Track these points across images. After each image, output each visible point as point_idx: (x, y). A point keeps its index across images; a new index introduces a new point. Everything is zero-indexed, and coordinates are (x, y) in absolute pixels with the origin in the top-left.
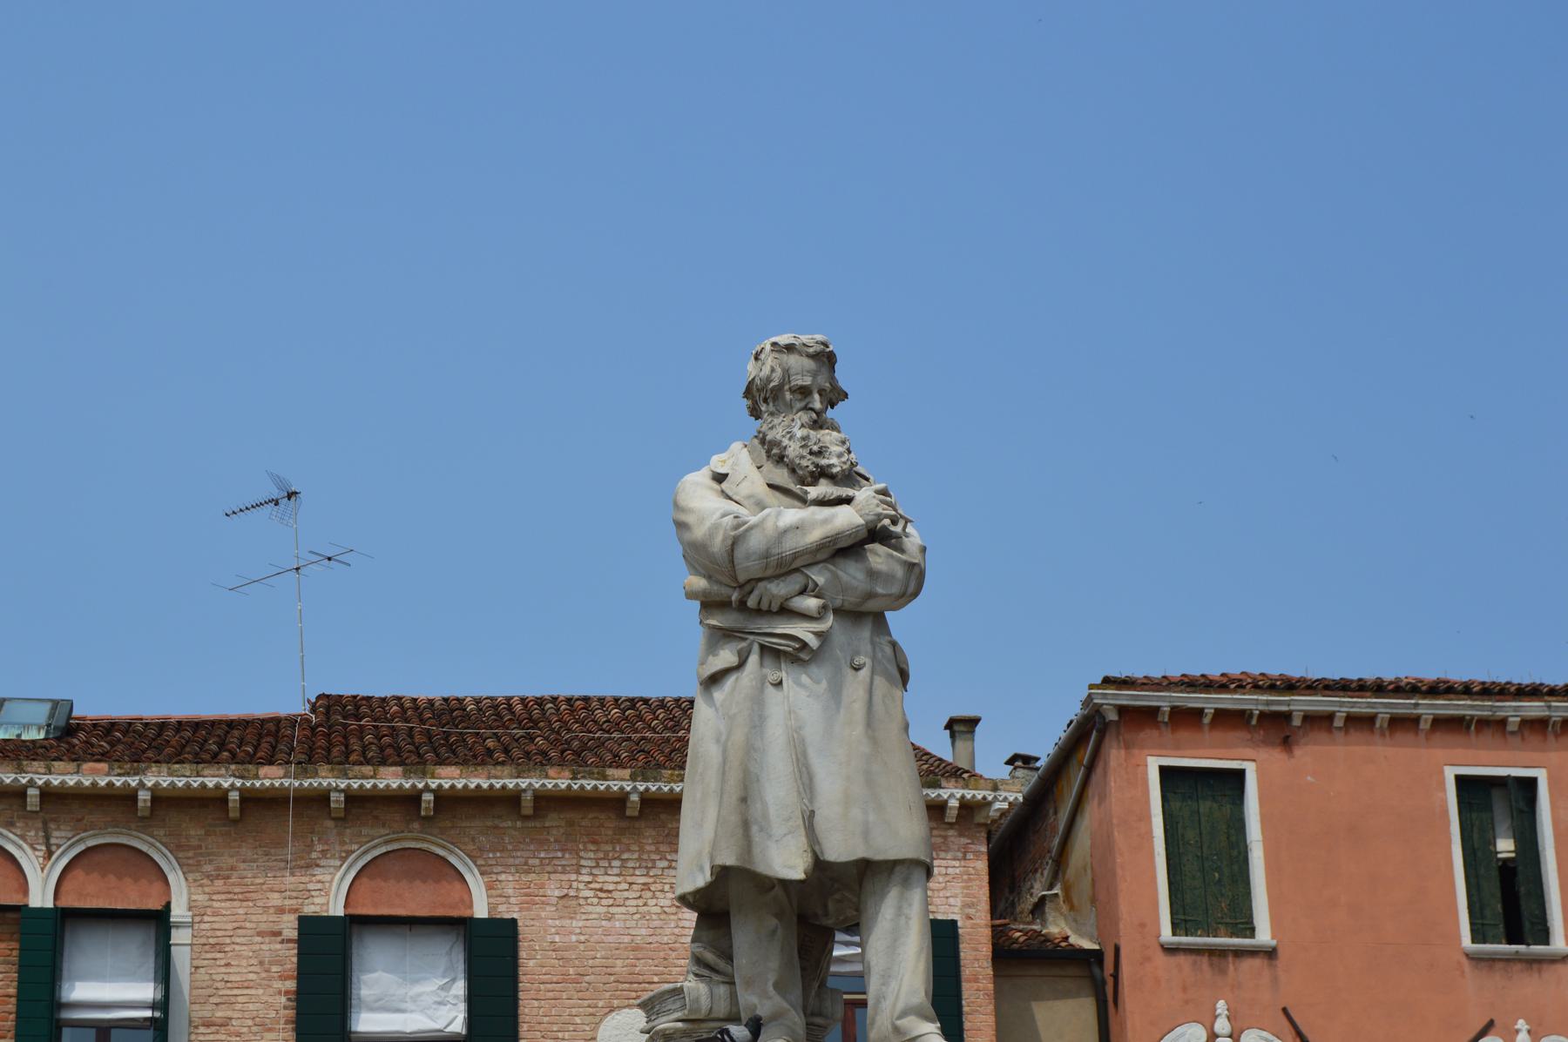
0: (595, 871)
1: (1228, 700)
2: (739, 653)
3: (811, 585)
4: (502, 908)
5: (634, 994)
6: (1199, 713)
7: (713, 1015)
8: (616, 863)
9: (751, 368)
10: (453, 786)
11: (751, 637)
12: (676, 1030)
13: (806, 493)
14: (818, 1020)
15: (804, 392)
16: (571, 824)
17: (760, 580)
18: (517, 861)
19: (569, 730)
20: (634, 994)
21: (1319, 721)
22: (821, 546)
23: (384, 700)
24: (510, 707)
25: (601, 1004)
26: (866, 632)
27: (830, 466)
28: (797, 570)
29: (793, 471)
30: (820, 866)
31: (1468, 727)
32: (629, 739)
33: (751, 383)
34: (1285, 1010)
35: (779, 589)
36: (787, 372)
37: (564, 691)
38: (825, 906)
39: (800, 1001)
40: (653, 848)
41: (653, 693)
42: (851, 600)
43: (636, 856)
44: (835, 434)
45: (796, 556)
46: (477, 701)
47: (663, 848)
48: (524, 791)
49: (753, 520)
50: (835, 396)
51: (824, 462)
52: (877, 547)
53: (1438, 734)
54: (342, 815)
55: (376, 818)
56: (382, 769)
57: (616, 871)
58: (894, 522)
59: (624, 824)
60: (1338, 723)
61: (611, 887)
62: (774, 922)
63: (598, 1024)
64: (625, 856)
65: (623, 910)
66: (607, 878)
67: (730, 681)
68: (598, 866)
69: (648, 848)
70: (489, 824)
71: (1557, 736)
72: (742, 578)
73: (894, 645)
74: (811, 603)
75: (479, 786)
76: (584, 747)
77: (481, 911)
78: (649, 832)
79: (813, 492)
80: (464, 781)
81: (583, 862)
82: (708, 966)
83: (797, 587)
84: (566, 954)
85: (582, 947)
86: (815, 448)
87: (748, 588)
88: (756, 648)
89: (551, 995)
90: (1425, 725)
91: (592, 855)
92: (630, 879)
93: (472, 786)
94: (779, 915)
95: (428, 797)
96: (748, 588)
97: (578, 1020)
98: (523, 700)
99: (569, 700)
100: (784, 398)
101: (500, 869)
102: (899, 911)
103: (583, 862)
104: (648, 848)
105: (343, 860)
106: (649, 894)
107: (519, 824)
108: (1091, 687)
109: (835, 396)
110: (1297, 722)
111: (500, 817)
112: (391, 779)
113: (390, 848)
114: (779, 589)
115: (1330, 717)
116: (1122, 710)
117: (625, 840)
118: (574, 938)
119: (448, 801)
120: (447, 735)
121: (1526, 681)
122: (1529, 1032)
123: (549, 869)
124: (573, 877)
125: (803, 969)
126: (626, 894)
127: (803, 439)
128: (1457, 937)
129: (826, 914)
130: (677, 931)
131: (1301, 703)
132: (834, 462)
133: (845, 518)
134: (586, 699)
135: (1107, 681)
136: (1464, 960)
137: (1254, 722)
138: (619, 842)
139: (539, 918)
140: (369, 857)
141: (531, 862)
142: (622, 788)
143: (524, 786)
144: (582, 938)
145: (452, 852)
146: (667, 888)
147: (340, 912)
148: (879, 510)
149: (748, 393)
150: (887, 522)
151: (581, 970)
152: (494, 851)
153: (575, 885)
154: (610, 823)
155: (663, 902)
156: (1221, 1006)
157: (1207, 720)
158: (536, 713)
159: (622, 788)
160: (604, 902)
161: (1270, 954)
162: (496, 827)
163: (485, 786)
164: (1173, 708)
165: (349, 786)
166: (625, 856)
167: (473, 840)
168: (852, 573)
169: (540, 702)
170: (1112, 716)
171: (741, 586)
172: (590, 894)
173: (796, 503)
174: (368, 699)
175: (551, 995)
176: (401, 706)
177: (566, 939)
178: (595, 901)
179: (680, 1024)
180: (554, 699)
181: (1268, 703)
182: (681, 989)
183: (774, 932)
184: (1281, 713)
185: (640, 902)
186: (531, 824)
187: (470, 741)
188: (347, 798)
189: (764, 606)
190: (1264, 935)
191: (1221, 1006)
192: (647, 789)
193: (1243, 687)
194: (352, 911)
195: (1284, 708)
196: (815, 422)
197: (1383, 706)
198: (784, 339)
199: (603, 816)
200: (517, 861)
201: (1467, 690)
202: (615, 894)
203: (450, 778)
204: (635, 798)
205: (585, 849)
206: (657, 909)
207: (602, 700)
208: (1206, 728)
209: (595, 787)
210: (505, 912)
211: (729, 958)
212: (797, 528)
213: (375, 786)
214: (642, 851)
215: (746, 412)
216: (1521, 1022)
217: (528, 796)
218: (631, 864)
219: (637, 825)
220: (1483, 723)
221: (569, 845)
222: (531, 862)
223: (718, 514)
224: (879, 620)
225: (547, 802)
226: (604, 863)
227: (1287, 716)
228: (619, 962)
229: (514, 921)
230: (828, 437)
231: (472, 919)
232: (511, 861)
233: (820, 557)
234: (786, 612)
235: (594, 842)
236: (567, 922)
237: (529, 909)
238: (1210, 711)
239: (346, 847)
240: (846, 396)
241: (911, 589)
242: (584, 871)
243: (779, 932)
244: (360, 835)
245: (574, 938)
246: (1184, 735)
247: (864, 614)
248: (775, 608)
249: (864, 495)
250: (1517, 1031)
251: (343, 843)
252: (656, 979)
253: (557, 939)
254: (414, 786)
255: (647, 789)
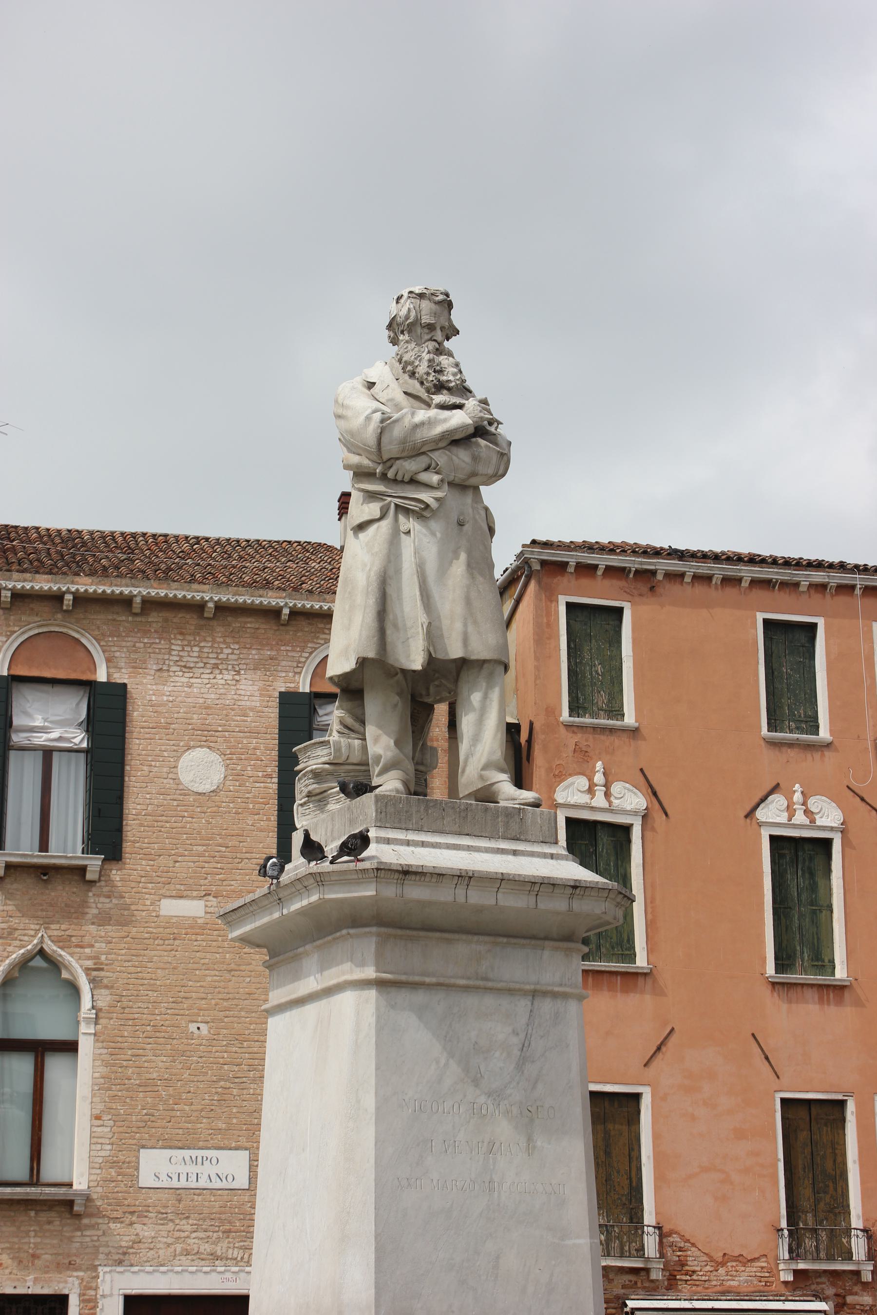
0: (181, 654)
1: (615, 560)
2: (381, 509)
3: (433, 465)
4: (116, 675)
5: (204, 738)
6: (595, 567)
7: (349, 761)
8: (196, 649)
9: (393, 309)
10: (86, 591)
11: (389, 499)
12: (324, 770)
13: (432, 399)
14: (421, 768)
15: (431, 327)
16: (166, 620)
17: (398, 459)
18: (128, 644)
19: (157, 556)
20: (204, 738)
21: (676, 577)
22: (443, 436)
23: (26, 528)
24: (114, 539)
25: (182, 744)
26: (469, 499)
27: (449, 381)
28: (424, 453)
29: (422, 383)
30: (431, 661)
31: (774, 587)
32: (198, 565)
33: (393, 319)
34: (641, 770)
35: (410, 466)
36: (419, 311)
37: (151, 529)
38: (428, 689)
39: (411, 754)
40: (221, 640)
41: (213, 534)
42: (460, 476)
43: (210, 644)
44: (451, 359)
45: (424, 443)
46: (91, 533)
47: (228, 640)
48: (135, 596)
49: (396, 416)
50: (452, 332)
51: (444, 378)
52: (480, 440)
53: (754, 590)
54: (9, 606)
55: (32, 609)
56: (37, 576)
57: (196, 654)
58: (490, 424)
59: (202, 622)
60: (688, 579)
61: (192, 665)
62: (397, 698)
63: (179, 757)
64: (202, 644)
65: (199, 680)
66: (189, 659)
67: (372, 530)
68: (183, 650)
69: (218, 639)
70: (110, 617)
71: (832, 596)
72: (385, 457)
73: (487, 509)
74: (435, 478)
75: (104, 591)
76: (169, 569)
77: (102, 676)
78: (219, 629)
79: (438, 399)
80: (94, 588)
81: (173, 647)
82: (346, 727)
83: (424, 466)
84: (159, 709)
85: (170, 705)
86: (438, 368)
87: (388, 464)
88: (393, 505)
89: (148, 736)
90: (745, 584)
91: (179, 642)
92: (205, 661)
93: (100, 591)
94: (400, 694)
95: (69, 597)
96: (388, 464)
97: (166, 754)
98: (122, 534)
99: (154, 536)
100: (416, 331)
101: (116, 649)
102: (485, 697)
103: (173, 647)
104: (218, 639)
105: (8, 637)
106: (217, 671)
107: (130, 618)
108: (524, 546)
109: (452, 332)
110: (660, 577)
111: (117, 613)
112: (43, 584)
113: (41, 630)
114: (410, 466)
115: (682, 575)
116: (543, 563)
117: (203, 634)
118: (165, 698)
119: (82, 600)
120: (74, 556)
121: (813, 557)
122: (802, 792)
123: (150, 650)
124: (166, 657)
125: (413, 732)
126: (201, 670)
127: (430, 361)
128: (760, 728)
129: (428, 695)
130: (235, 697)
131: (663, 565)
132: (449, 376)
133: (458, 419)
134: (166, 536)
135: (534, 542)
136: (762, 743)
137: (631, 575)
138: (198, 634)
139: (142, 683)
140: (26, 636)
141: (137, 645)
142: (202, 598)
143: (135, 593)
144: (171, 699)
145: (83, 635)
146: (230, 667)
147: (307, 690)
148: (482, 414)
149: (390, 327)
150: (486, 423)
151: (169, 720)
152: (112, 636)
153: (167, 662)
154: (191, 621)
155: (226, 677)
156: (599, 765)
157: (600, 573)
158: (132, 544)
159: (202, 598)
160: (187, 675)
161: (634, 732)
162: (114, 620)
163: (109, 591)
164: (578, 563)
165: (14, 586)
166: (202, 644)
167: (98, 628)
168: (462, 456)
169: (134, 535)
170: (536, 567)
171: (384, 463)
172: (178, 669)
173: (423, 406)
174: (16, 527)
175: (148, 736)
176: (39, 533)
177: (160, 699)
178: (181, 674)
179: (327, 766)
180: (144, 535)
181: (641, 563)
182: (328, 742)
183: (396, 705)
184: (648, 571)
185: (212, 676)
186: (139, 619)
187: (91, 560)
188: (12, 594)
189: (399, 478)
190: (630, 719)
191: (599, 765)
192: (295, 605)
193: (626, 552)
194: (13, 672)
195: (652, 567)
196: (437, 349)
197: (718, 570)
198: (417, 290)
199: (188, 616)
200: (128, 644)
201: (774, 562)
202: (194, 670)
203: (86, 585)
204: (211, 605)
205: (175, 639)
206: (223, 682)
207: (176, 537)
208: (599, 578)
209: (184, 596)
210: (119, 678)
211: (363, 722)
212: (430, 423)
213: (32, 587)
214: (214, 641)
215: (387, 340)
216: (797, 785)
217: (138, 600)
218: (206, 650)
219: (211, 623)
220: (784, 585)
221: (165, 635)
222: (137, 645)
223: (369, 411)
224: (476, 489)
225: (151, 604)
226: (187, 648)
227: (653, 573)
228: (195, 716)
229: (125, 685)
230: (444, 360)
231: (95, 682)
232: (124, 644)
233: (441, 445)
234: (413, 482)
235: (181, 634)
236: (160, 687)
237: (135, 677)
238: (602, 567)
239: (11, 629)
240: (458, 332)
241: (500, 472)
242: (174, 653)
243: (400, 705)
244: (20, 620)
245: (165, 698)
246: (585, 582)
247: (466, 486)
248: (407, 479)
249: (471, 404)
250: (794, 792)
251: (8, 625)
252: (220, 729)
253: (154, 698)
254: (59, 589)
255: (295, 605)
